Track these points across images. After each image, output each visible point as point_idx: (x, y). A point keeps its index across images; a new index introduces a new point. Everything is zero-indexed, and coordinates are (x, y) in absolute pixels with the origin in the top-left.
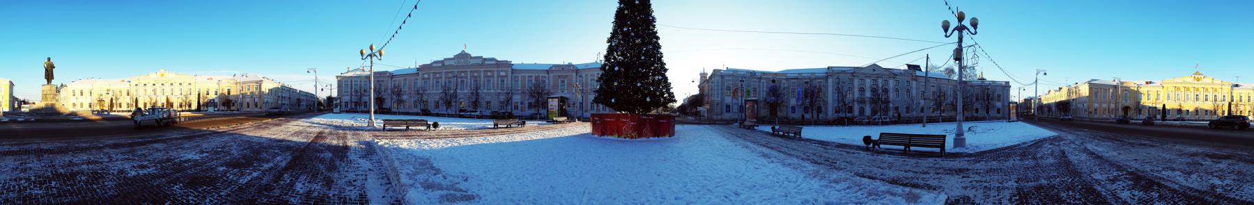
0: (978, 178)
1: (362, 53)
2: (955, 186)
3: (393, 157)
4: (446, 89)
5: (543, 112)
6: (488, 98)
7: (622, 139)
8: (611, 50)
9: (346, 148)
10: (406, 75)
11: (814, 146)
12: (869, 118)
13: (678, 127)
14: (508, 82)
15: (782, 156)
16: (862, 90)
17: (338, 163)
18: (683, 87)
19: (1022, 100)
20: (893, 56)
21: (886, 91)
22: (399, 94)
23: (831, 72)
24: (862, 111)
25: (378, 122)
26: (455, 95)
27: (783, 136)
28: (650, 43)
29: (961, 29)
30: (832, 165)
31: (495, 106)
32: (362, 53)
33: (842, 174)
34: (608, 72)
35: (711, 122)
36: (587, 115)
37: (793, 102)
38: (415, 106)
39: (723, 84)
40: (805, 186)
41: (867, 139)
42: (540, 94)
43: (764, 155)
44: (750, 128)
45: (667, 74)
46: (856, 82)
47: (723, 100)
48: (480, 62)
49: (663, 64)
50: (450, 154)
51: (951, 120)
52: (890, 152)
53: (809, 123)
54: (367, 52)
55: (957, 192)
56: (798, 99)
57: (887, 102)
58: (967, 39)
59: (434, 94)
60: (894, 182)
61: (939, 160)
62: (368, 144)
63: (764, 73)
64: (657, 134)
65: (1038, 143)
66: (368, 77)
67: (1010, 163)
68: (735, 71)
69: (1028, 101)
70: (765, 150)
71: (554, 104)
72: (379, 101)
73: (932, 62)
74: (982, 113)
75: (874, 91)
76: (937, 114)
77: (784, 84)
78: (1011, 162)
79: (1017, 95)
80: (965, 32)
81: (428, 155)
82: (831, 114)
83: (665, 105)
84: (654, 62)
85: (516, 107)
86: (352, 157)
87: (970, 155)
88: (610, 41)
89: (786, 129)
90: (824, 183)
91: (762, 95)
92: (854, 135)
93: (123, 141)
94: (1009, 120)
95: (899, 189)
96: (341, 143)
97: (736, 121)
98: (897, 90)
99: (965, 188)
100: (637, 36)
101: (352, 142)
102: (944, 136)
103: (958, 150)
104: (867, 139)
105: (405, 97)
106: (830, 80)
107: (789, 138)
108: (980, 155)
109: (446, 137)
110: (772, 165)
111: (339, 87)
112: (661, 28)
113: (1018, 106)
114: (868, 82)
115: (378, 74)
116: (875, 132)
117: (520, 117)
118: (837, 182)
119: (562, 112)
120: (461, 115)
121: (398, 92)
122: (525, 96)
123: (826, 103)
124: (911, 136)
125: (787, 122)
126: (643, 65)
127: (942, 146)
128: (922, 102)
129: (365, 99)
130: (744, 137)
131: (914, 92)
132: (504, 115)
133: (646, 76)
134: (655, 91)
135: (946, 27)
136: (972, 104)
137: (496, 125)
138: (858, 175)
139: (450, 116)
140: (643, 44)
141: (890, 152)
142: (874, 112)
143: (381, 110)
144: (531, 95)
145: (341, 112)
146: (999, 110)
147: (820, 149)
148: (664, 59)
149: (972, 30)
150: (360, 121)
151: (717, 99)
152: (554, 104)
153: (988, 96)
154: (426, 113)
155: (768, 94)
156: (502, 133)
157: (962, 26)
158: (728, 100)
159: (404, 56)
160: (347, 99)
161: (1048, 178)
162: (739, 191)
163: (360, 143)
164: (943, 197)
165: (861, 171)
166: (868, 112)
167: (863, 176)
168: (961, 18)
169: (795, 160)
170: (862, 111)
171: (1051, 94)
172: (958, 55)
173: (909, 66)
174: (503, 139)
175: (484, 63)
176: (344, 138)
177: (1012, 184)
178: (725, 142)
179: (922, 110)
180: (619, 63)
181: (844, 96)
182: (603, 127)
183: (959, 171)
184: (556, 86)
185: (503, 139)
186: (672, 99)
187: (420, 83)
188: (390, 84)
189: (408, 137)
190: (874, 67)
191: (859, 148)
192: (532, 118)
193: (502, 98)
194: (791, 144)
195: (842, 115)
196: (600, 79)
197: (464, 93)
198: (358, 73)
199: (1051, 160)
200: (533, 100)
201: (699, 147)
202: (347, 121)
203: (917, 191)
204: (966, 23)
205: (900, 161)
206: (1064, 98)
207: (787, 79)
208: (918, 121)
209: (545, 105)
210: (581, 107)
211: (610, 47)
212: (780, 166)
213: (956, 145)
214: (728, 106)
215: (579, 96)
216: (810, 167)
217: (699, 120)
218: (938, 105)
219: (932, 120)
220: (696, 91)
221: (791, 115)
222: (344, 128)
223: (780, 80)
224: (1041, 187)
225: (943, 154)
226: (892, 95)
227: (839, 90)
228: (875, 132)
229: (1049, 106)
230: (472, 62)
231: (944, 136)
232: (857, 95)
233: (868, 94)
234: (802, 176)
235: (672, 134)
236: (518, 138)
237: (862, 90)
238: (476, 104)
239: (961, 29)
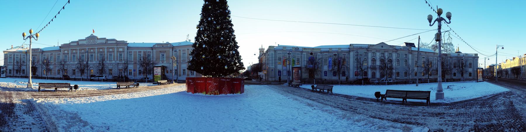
0: (450, 118)
1: (24, 35)
2: (435, 123)
3: (50, 112)
4: (81, 60)
5: (150, 77)
6: (110, 67)
7: (208, 95)
8: (199, 33)
9: (13, 105)
10: (52, 52)
11: (341, 99)
12: (379, 79)
13: (246, 87)
14: (125, 56)
15: (321, 105)
16: (374, 60)
17: (7, 118)
18: (249, 58)
19: (487, 67)
20: (397, 39)
21: (391, 61)
22: (47, 64)
23: (352, 48)
24: (374, 75)
25: (35, 85)
26: (87, 65)
27: (319, 92)
28: (226, 28)
29: (440, 20)
30: (354, 110)
31: (115, 73)
32: (24, 35)
33: (362, 117)
34: (197, 49)
35: (268, 83)
36: (184, 78)
37: (325, 68)
38: (59, 73)
39: (275, 57)
40: (338, 124)
41: (378, 94)
42: (148, 64)
43: (309, 105)
44: (297, 86)
45: (239, 50)
46: (370, 55)
47: (276, 67)
48: (104, 41)
49: (236, 43)
50: (94, 108)
51: (435, 81)
52: (393, 103)
53: (337, 83)
54: (27, 34)
55: (435, 127)
56: (329, 66)
57: (391, 68)
58: (444, 26)
59: (72, 64)
60: (395, 121)
61: (425, 108)
62: (29, 102)
63: (305, 48)
64: (232, 92)
65: (495, 97)
66: (27, 52)
67: (473, 110)
68: (284, 47)
69: (492, 67)
70: (309, 101)
71: (158, 71)
72: (34, 69)
73: (422, 41)
74: (458, 76)
75: (382, 61)
76: (426, 77)
77: (319, 56)
78: (474, 109)
79: (483, 64)
80: (443, 22)
81: (76, 111)
82: (352, 77)
83: (237, 71)
84: (230, 42)
85: (130, 73)
86: (18, 113)
87: (447, 104)
88: (198, 27)
89: (322, 87)
90: (350, 122)
91: (304, 63)
92: (369, 91)
93: (83, 100)
94: (477, 80)
95: (399, 125)
96: (8, 101)
97: (286, 81)
98: (398, 61)
99: (441, 125)
100: (218, 24)
101: (16, 101)
102: (429, 92)
103: (439, 101)
104: (378, 94)
105: (51, 67)
106: (352, 53)
107: (324, 93)
108: (454, 105)
109: (85, 96)
110: (315, 111)
111: (6, 59)
112: (234, 18)
113: (483, 71)
114: (378, 55)
115: (33, 49)
116: (383, 90)
117: (134, 80)
118: (358, 121)
119: (164, 77)
120: (92, 79)
121: (47, 63)
122: (140, 66)
123: (348, 69)
124: (407, 92)
125: (321, 82)
126: (222, 44)
127: (428, 99)
128: (416, 69)
129: (23, 67)
130: (293, 93)
131: (410, 62)
132: (122, 78)
133: (223, 51)
134: (230, 62)
135: (430, 19)
136: (451, 70)
137: (118, 86)
138: (372, 117)
139: (83, 80)
140: (222, 29)
141: (393, 103)
142: (382, 76)
143: (35, 77)
144: (142, 65)
145: (6, 77)
146: (470, 74)
147: (345, 100)
148: (237, 40)
149: (448, 20)
150: (22, 84)
151: (272, 66)
152: (158, 71)
153: (462, 64)
154: (66, 78)
155: (308, 62)
156: (124, 92)
157: (440, 18)
158: (280, 67)
159: (52, 38)
160: (10, 67)
161: (498, 120)
162: (296, 128)
163: (23, 101)
164: (426, 129)
165: (373, 114)
166: (378, 75)
167: (375, 118)
168: (440, 12)
169: (330, 108)
170: (374, 75)
171: (507, 61)
172: (438, 38)
173: (407, 44)
174: (126, 96)
175: (106, 42)
176: (10, 97)
177: (472, 123)
178: (281, 97)
179: (416, 75)
180: (205, 42)
181: (361, 65)
182: (195, 87)
183: (438, 115)
184: (158, 58)
185: (126, 96)
186: (242, 67)
187: (62, 57)
188: (40, 57)
189: (57, 96)
190: (382, 44)
191: (372, 100)
192: (143, 81)
193: (121, 67)
194: (326, 97)
195: (360, 77)
196: (192, 53)
197: (94, 63)
198: (21, 49)
199: (503, 108)
200: (142, 69)
201: (261, 99)
202: (11, 83)
203: (411, 126)
204: (444, 16)
205: (399, 108)
206: (517, 65)
207: (321, 52)
208: (413, 82)
209: (151, 71)
210: (176, 73)
211: (199, 32)
212: (319, 111)
213: (437, 98)
214: (279, 72)
215: (175, 65)
216: (340, 112)
217: (260, 81)
218: (427, 71)
219: (422, 81)
220: (257, 61)
221: (324, 78)
222: (10, 89)
223: (316, 53)
224: (492, 125)
225: (428, 104)
226: (394, 64)
227: (357, 60)
228: (383, 90)
229: (506, 71)
230: (99, 42)
231: (429, 92)
232: (370, 63)
233: (378, 63)
234: (335, 118)
235: (242, 92)
236: (136, 95)
237: (374, 60)
238: (102, 71)
239: (440, 20)
